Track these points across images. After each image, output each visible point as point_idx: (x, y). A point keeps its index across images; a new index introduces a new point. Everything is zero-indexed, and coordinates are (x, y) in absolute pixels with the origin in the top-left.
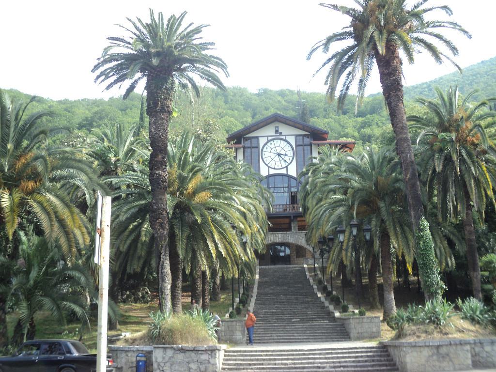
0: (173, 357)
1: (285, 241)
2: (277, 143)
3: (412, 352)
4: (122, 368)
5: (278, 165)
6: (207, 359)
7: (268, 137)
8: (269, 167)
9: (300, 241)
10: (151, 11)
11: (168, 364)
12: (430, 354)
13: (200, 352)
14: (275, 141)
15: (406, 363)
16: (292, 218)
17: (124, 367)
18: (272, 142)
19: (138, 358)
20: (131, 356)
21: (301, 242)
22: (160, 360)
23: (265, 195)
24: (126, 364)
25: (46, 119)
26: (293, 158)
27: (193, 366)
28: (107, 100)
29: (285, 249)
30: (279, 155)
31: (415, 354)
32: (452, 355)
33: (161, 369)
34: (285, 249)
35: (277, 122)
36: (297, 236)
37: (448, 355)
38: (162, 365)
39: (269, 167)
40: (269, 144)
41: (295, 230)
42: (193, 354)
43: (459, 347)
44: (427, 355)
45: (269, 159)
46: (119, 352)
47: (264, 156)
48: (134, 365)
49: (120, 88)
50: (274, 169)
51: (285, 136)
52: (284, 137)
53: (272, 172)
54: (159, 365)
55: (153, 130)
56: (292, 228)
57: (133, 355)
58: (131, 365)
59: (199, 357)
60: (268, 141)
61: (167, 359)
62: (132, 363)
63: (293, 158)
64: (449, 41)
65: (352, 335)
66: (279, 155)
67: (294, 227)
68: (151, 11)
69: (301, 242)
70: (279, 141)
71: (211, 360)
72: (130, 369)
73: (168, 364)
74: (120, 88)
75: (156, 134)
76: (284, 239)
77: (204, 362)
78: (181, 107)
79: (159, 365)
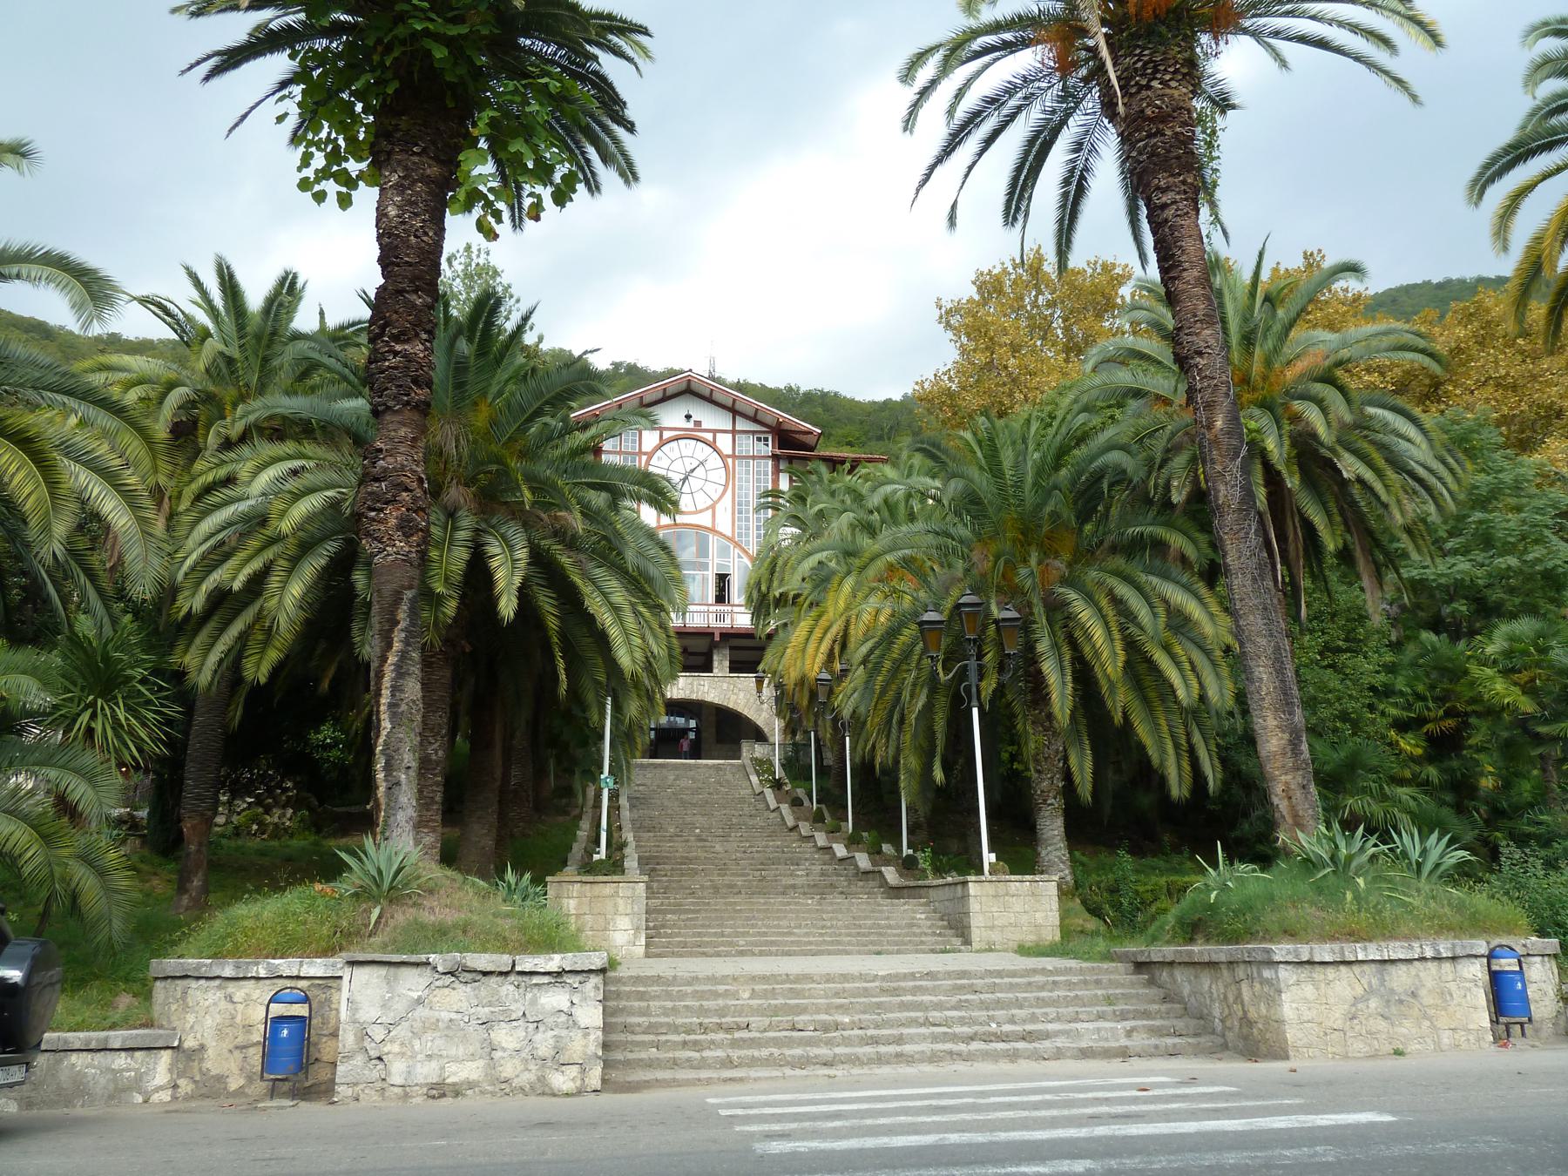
0: (420, 1001)
1: (694, 697)
3: (1298, 983)
4: (202, 1047)
6: (565, 1006)
9: (733, 698)
12: (1359, 991)
13: (536, 980)
15: (1280, 1022)
16: (717, 638)
17: (211, 1044)
19: (277, 1009)
20: (247, 1000)
22: (368, 1013)
23: (262, 973)
24: (220, 1033)
26: (726, 486)
31: (1309, 990)
32: (1427, 999)
33: (374, 1054)
37: (1414, 995)
38: (378, 1033)
41: (721, 670)
43: (1447, 966)
44: (1348, 993)
45: (709, 488)
46: (194, 984)
48: (257, 1037)
51: (715, 432)
52: (709, 436)
54: (363, 1035)
55: (392, 211)
56: (716, 664)
57: (256, 994)
59: (534, 1002)
60: (663, 443)
61: (400, 1007)
62: (248, 1028)
63: (726, 486)
65: (976, 935)
72: (237, 1053)
73: (401, 1031)
75: (403, 223)
77: (550, 1020)
79: (363, 1035)
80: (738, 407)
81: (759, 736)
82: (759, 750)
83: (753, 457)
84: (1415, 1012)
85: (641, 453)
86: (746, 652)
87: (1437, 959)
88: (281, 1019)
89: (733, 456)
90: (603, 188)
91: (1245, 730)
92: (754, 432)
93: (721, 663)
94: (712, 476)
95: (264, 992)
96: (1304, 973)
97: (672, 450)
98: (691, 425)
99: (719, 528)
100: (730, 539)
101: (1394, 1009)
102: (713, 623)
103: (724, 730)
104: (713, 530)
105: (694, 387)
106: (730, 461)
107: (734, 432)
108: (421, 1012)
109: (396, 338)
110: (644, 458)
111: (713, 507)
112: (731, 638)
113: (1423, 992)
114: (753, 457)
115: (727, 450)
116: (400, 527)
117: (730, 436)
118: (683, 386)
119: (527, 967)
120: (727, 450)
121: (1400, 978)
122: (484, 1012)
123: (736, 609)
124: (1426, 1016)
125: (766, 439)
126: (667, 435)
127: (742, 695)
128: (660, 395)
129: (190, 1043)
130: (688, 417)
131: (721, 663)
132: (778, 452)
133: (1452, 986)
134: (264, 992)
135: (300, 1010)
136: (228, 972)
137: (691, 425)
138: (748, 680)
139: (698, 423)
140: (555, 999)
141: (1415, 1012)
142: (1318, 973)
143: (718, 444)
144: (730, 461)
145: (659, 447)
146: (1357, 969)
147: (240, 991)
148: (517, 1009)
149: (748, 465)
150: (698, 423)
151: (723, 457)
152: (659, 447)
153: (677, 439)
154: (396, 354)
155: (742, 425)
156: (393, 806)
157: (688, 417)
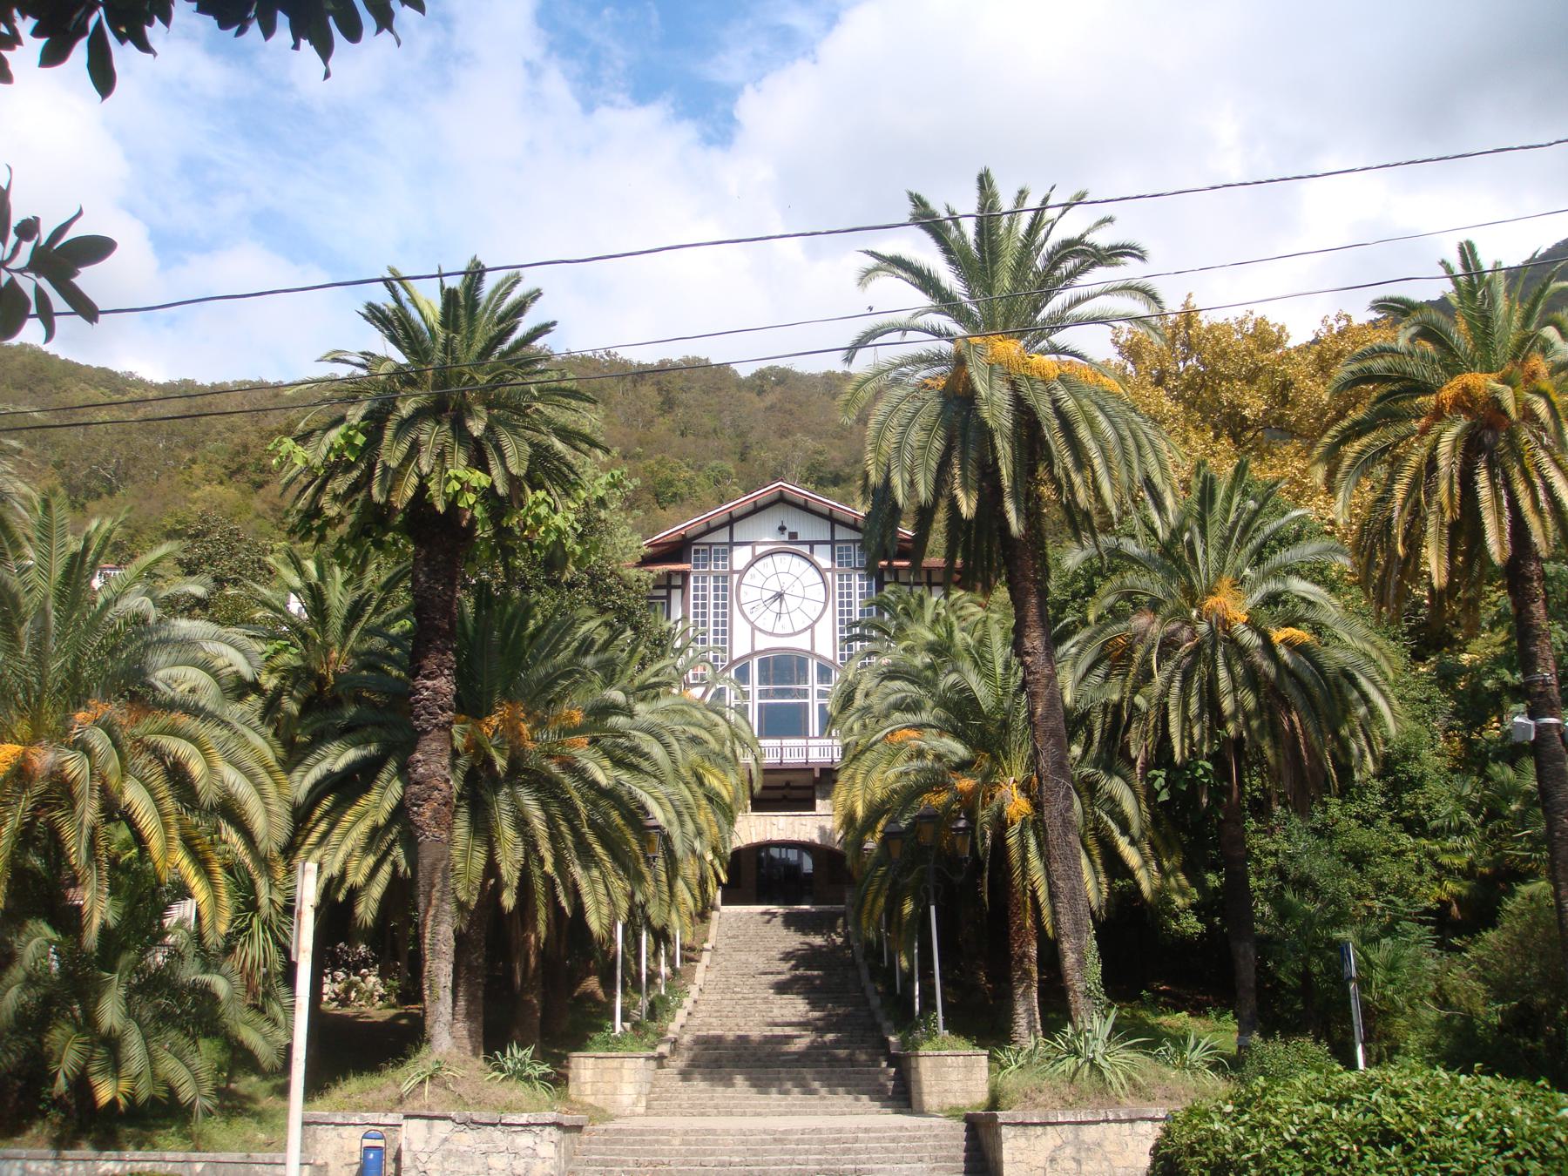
0: (446, 1140)
2: (783, 561)
6: (531, 1144)
8: (754, 628)
10: (984, 182)
11: (437, 1157)
14: (777, 558)
16: (817, 775)
17: (331, 1162)
18: (768, 560)
19: (368, 1143)
24: (336, 1156)
25: (336, 498)
27: (498, 1162)
29: (800, 857)
30: (780, 596)
31: (1022, 1142)
32: (1109, 1147)
34: (800, 857)
38: (424, 1157)
39: (754, 628)
42: (496, 1134)
45: (807, 605)
47: (743, 599)
50: (772, 634)
51: (812, 544)
53: (763, 643)
54: (415, 1158)
58: (348, 1160)
59: (513, 1141)
60: (757, 559)
61: (435, 1143)
62: (351, 1153)
66: (780, 596)
68: (984, 182)
70: (788, 558)
71: (538, 1148)
73: (437, 1157)
77: (522, 1153)
79: (415, 1158)
80: (836, 514)
84: (1099, 1156)
85: (733, 572)
87: (1107, 1121)
88: (368, 1148)
91: (246, 1110)
92: (854, 542)
94: (810, 593)
95: (360, 1132)
96: (1019, 1130)
97: (753, 576)
99: (818, 651)
101: (1083, 1154)
104: (812, 653)
106: (829, 575)
107: (832, 542)
108: (447, 1146)
109: (427, 677)
110: (736, 577)
111: (811, 627)
113: (1106, 1143)
116: (433, 818)
118: (776, 496)
119: (508, 1121)
121: (1090, 1133)
122: (484, 1147)
124: (1106, 1159)
126: (760, 550)
128: (751, 507)
129: (320, 1162)
133: (1128, 1139)
134: (360, 1132)
135: (380, 1143)
136: (339, 1120)
137: (786, 537)
139: (793, 535)
140: (525, 1140)
141: (1099, 1156)
142: (1031, 1131)
145: (751, 565)
146: (1059, 1128)
147: (347, 1131)
148: (503, 1145)
150: (793, 535)
152: (751, 565)
153: (770, 554)
154: (427, 689)
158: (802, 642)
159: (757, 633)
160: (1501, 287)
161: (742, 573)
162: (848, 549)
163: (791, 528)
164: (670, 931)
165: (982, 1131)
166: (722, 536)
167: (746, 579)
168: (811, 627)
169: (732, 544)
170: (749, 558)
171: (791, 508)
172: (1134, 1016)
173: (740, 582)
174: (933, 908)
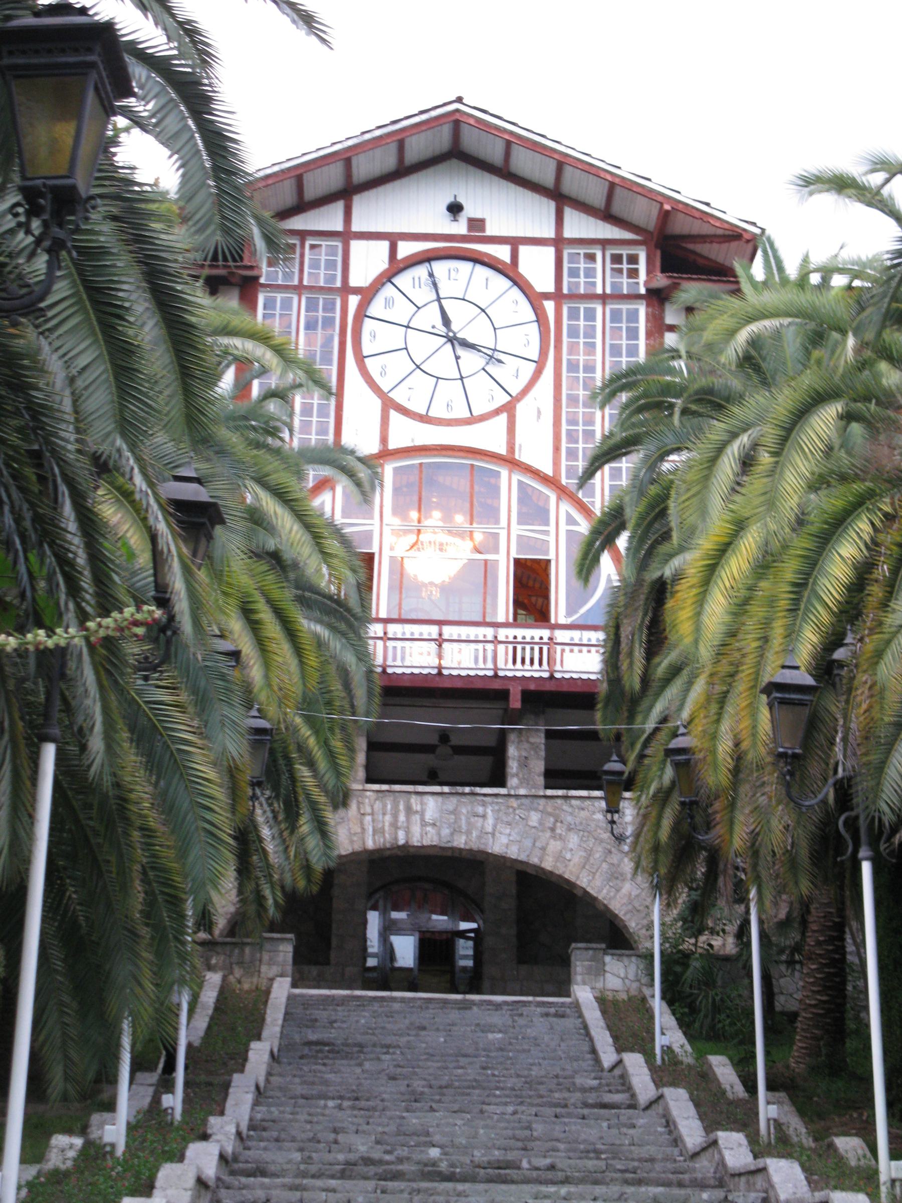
1: (460, 842)
5: (449, 401)
7: (393, 239)
8: (389, 404)
9: (554, 846)
16: (516, 702)
21: (559, 857)
28: (250, 168)
35: (454, 162)
36: (534, 818)
39: (389, 404)
40: (403, 280)
47: (367, 348)
49: (539, 412)
50: (425, 419)
51: (515, 243)
52: (503, 253)
53: (404, 432)
56: (513, 766)
60: (397, 267)
63: (538, 373)
64: (189, 22)
67: (524, 763)
69: (559, 857)
70: (465, 267)
74: (539, 412)
76: (455, 831)
78: (539, 1129)
81: (615, 937)
82: (618, 974)
83: (604, 298)
85: (346, 290)
86: (577, 734)
89: (558, 296)
90: (133, 163)
92: (604, 243)
93: (525, 756)
97: (389, 303)
98: (460, 228)
99: (524, 456)
100: (551, 481)
102: (508, 669)
103: (534, 926)
104: (510, 461)
105: (471, 141)
106: (549, 306)
107: (559, 242)
110: (354, 301)
111: (509, 409)
112: (552, 700)
114: (604, 298)
115: (544, 282)
117: (549, 252)
118: (442, 140)
120: (544, 282)
123: (562, 636)
125: (633, 259)
126: (405, 249)
127: (574, 840)
130: (455, 209)
131: (525, 756)
132: (70, 616)
138: (588, 805)
139: (476, 224)
143: (523, 269)
144: (549, 306)
145: (388, 277)
149: (590, 315)
150: (476, 224)
151: (535, 299)
152: (388, 277)
155: (578, 226)
156: (64, 502)
157: (455, 209)
158: (490, 437)
159: (393, 414)
160: (227, 1077)
161: (368, 294)
162: (591, 258)
163: (471, 210)
164: (702, 699)
165: (325, 393)
166: (330, 219)
167: (376, 308)
168: (509, 409)
169: (346, 236)
170: (382, 264)
171: (479, 173)
172: (517, 775)
173: (361, 314)
174: (866, 868)
